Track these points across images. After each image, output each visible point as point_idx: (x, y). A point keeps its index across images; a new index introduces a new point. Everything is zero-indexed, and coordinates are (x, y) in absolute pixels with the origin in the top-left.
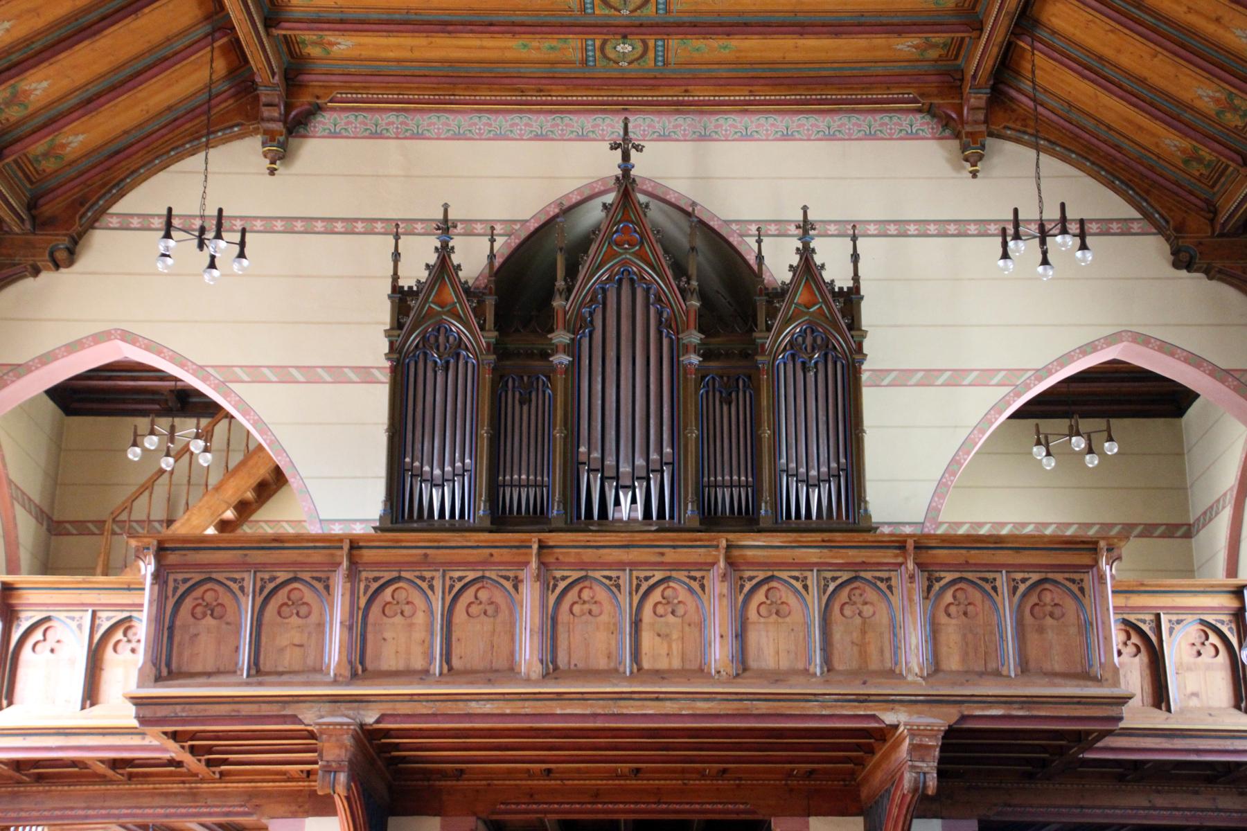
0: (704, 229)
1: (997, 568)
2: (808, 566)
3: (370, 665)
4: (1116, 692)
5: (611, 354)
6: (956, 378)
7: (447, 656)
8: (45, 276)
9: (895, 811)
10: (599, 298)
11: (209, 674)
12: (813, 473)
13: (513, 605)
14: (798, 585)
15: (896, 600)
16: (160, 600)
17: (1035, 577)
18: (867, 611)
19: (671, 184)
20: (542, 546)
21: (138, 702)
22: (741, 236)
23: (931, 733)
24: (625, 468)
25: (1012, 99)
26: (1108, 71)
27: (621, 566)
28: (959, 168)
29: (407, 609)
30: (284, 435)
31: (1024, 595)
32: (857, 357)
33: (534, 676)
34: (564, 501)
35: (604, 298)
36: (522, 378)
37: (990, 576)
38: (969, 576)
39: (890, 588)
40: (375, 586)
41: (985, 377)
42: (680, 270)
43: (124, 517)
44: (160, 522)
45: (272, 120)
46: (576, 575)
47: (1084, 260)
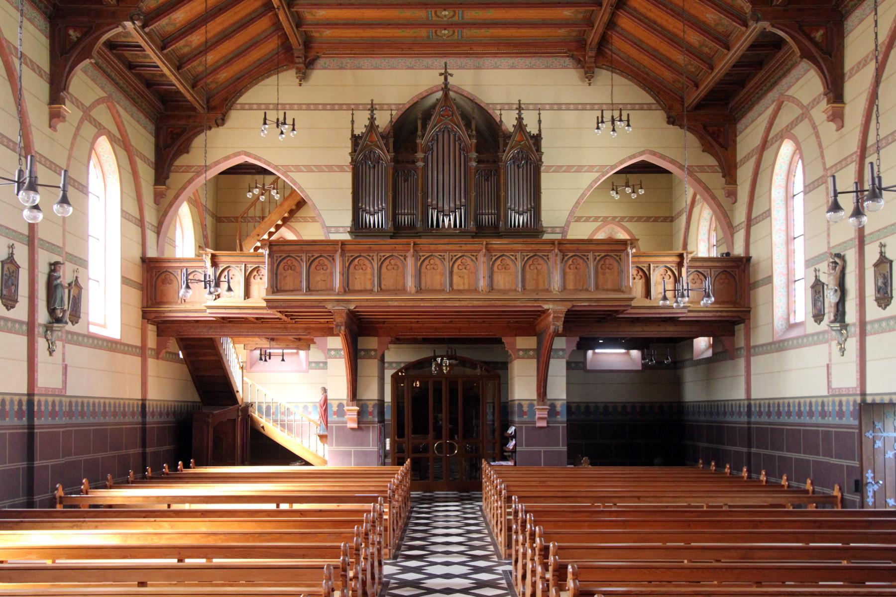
0: (478, 106)
1: (589, 251)
2: (517, 251)
3: (351, 288)
4: (630, 296)
5: (440, 162)
6: (579, 169)
7: (380, 285)
8: (213, 130)
9: (547, 337)
10: (435, 139)
11: (292, 291)
12: (521, 209)
13: (404, 265)
14: (513, 258)
15: (550, 263)
16: (271, 264)
17: (603, 254)
18: (539, 267)
19: (464, 88)
20: (415, 244)
21: (266, 300)
22: (494, 110)
23: (561, 313)
24: (446, 208)
25: (606, 52)
26: (643, 46)
27: (445, 251)
28: (583, 81)
29: (364, 267)
30: (309, 192)
31: (599, 261)
32: (539, 163)
33: (413, 292)
34: (422, 221)
35: (437, 138)
36: (404, 171)
37: (586, 254)
38: (579, 254)
39: (548, 259)
40: (352, 258)
41: (590, 169)
42: (468, 125)
43: (245, 215)
44: (259, 217)
45: (299, 63)
46: (428, 254)
47: (628, 130)
